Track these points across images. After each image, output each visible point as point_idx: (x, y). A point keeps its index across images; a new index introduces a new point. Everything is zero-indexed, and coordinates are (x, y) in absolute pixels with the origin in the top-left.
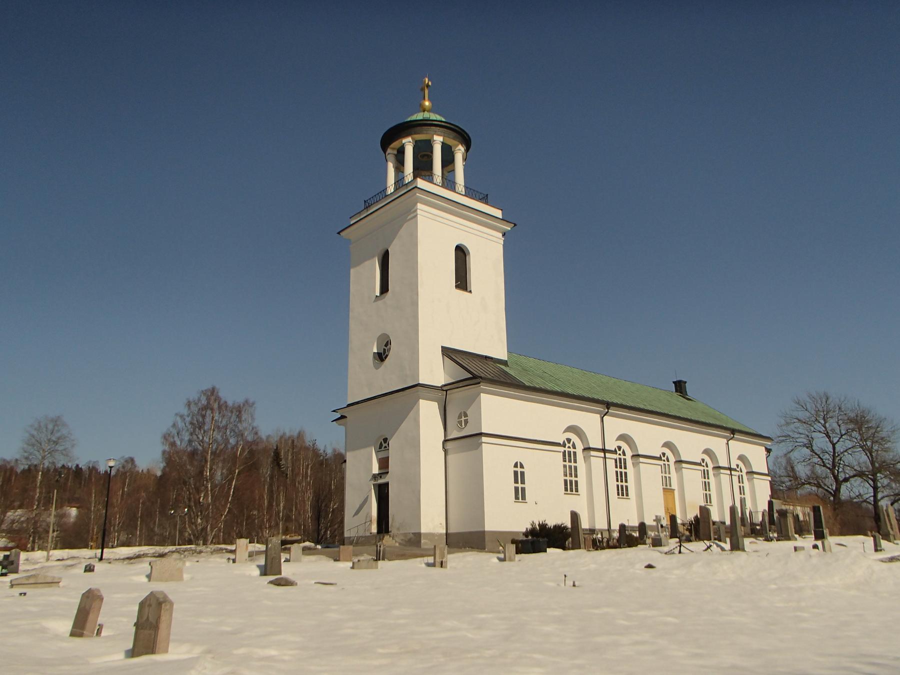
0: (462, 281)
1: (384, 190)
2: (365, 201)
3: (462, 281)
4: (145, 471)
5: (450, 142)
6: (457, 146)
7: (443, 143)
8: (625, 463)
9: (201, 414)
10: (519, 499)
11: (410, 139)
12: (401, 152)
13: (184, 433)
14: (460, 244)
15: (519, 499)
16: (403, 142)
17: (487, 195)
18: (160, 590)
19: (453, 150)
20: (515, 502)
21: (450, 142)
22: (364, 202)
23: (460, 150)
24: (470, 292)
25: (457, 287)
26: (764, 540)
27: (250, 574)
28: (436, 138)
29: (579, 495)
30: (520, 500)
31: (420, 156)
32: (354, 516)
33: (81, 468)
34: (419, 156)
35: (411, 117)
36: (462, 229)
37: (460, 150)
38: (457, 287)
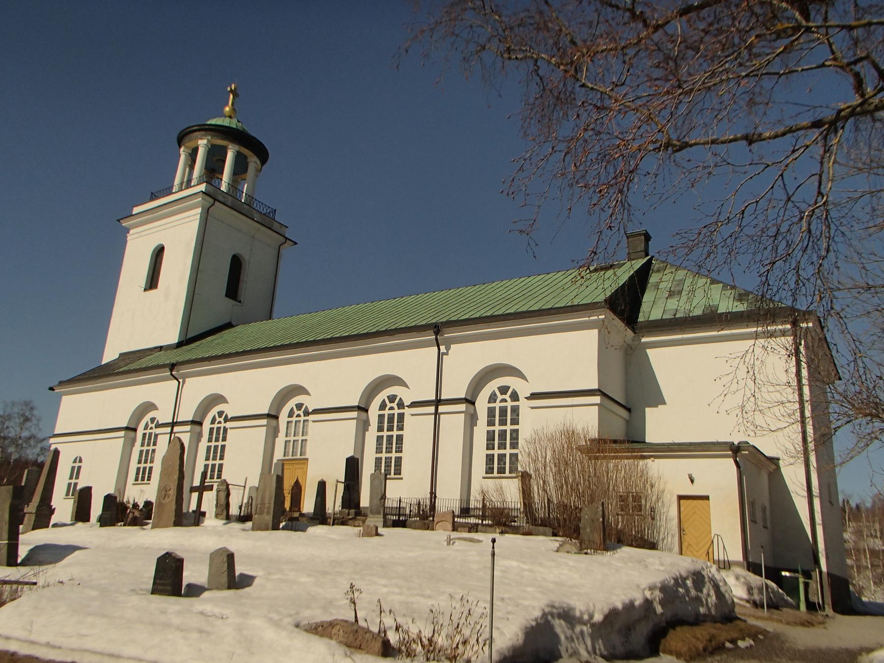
0: (152, 282)
1: (169, 188)
2: (152, 193)
3: (152, 282)
4: (53, 507)
8: (138, 473)
10: (505, 473)
11: (205, 142)
12: (195, 151)
14: (238, 254)
15: (505, 473)
17: (275, 210)
20: (484, 478)
22: (150, 194)
24: (240, 302)
25: (227, 295)
26: (253, 529)
29: (402, 479)
30: (495, 474)
31: (216, 160)
35: (216, 119)
36: (159, 228)
38: (227, 295)
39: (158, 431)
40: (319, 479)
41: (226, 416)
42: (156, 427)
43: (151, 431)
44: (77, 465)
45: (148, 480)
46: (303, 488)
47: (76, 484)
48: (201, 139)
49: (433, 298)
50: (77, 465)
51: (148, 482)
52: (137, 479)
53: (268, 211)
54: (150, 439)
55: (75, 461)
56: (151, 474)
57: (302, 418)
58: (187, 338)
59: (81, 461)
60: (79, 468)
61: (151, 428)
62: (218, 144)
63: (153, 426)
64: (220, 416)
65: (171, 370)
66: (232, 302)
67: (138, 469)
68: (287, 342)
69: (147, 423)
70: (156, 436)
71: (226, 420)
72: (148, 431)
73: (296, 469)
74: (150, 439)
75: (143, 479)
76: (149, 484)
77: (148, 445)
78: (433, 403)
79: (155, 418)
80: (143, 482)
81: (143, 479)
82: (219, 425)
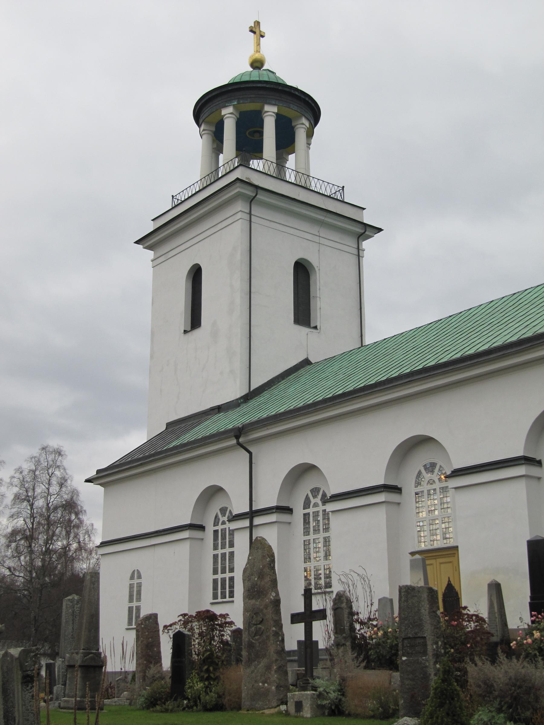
2: (173, 196)
5: (289, 112)
6: (299, 118)
7: (277, 114)
8: (215, 588)
9: (43, 647)
11: (230, 109)
13: (60, 659)
16: (223, 113)
17: (343, 187)
18: (304, 358)
19: (293, 124)
21: (289, 112)
23: (303, 124)
24: (315, 328)
27: (42, 660)
28: (267, 108)
31: (249, 133)
32: (449, 578)
33: (516, 659)
34: (247, 133)
37: (303, 124)
39: (234, 525)
40: (488, 579)
41: (324, 495)
42: (229, 521)
43: (223, 527)
44: (135, 581)
45: (230, 597)
46: (459, 593)
47: (138, 609)
48: (225, 107)
49: (250, 406)
50: (135, 581)
51: (231, 599)
52: (215, 596)
53: (333, 191)
54: (223, 538)
55: (132, 578)
56: (233, 587)
57: (321, 508)
58: (252, 389)
59: (139, 577)
60: (139, 585)
61: (224, 523)
62: (248, 109)
63: (225, 519)
64: (224, 514)
65: (237, 437)
66: (304, 330)
67: (215, 581)
68: (395, 373)
69: (216, 517)
70: (232, 532)
71: (325, 500)
72: (220, 527)
73: (441, 563)
74: (223, 538)
75: (223, 596)
76: (233, 602)
77: (223, 547)
78: (248, 516)
79: (227, 508)
80: (224, 600)
81: (223, 596)
82: (316, 509)
